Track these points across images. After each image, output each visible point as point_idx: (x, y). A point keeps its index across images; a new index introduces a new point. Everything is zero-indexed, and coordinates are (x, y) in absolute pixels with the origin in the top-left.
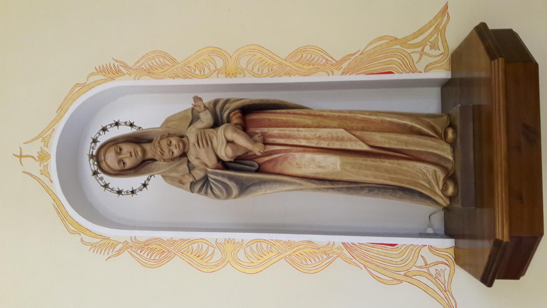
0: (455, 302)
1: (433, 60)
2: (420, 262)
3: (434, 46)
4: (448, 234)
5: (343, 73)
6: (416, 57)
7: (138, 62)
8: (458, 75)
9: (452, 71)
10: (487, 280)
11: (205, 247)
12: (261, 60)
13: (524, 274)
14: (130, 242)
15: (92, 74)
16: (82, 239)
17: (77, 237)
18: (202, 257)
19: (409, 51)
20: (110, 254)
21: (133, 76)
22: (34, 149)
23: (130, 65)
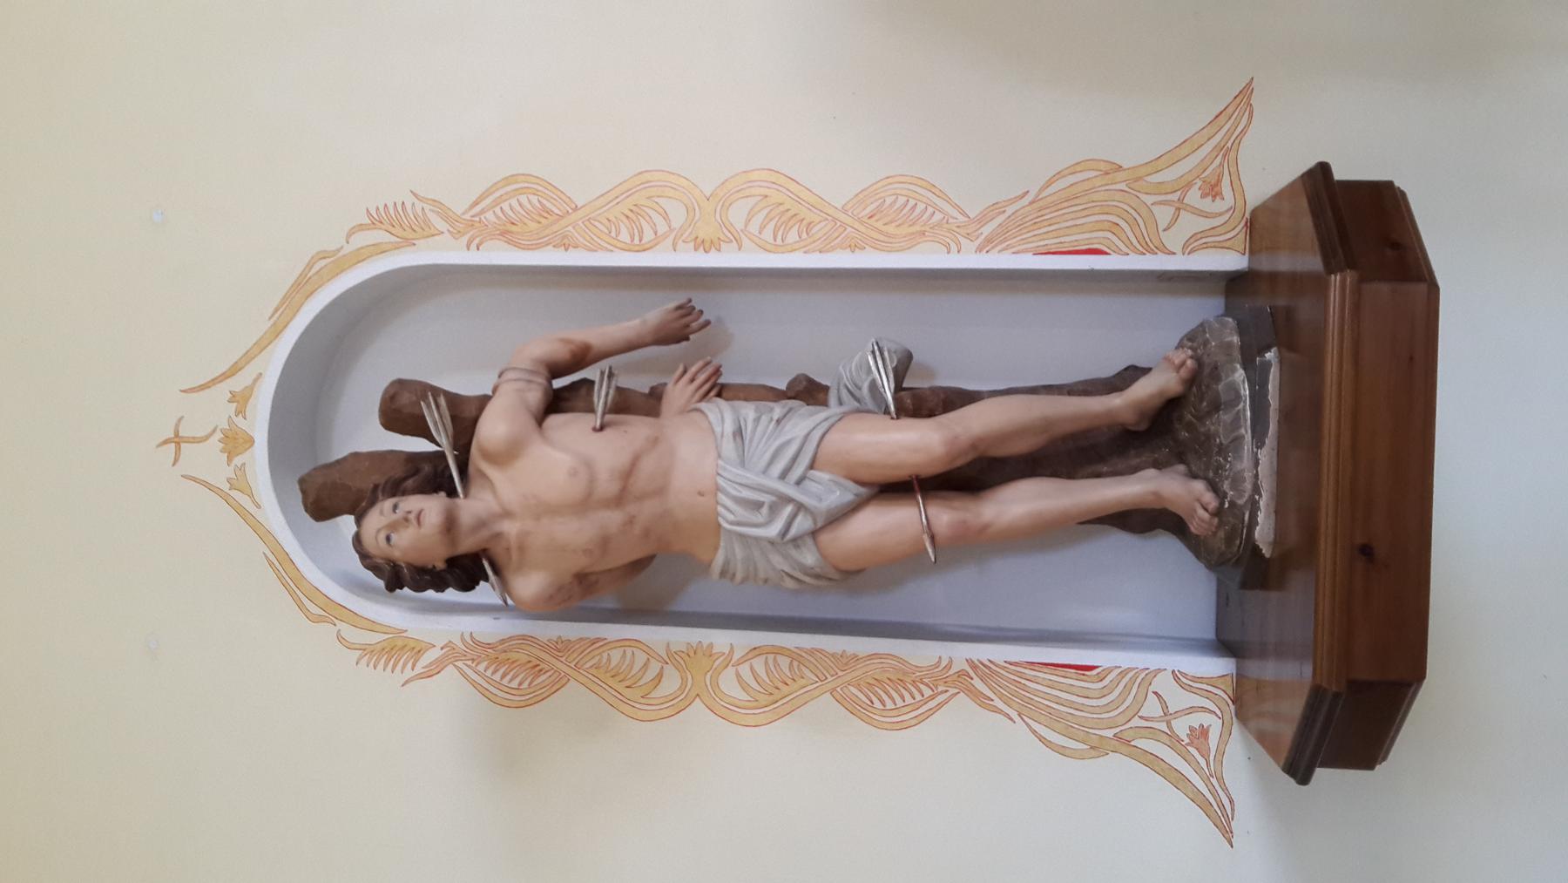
0: (1231, 801)
1: (1206, 224)
2: (1152, 708)
3: (1213, 191)
4: (1225, 645)
5: (979, 249)
6: (1163, 215)
7: (476, 203)
8: (1266, 264)
9: (1252, 252)
10: (1299, 768)
11: (641, 658)
12: (782, 208)
13: (1384, 759)
14: (460, 645)
15: (361, 227)
16: (340, 638)
17: (326, 631)
18: (628, 683)
19: (1149, 200)
20: (409, 673)
21: (465, 239)
22: (213, 411)
23: (459, 206)
